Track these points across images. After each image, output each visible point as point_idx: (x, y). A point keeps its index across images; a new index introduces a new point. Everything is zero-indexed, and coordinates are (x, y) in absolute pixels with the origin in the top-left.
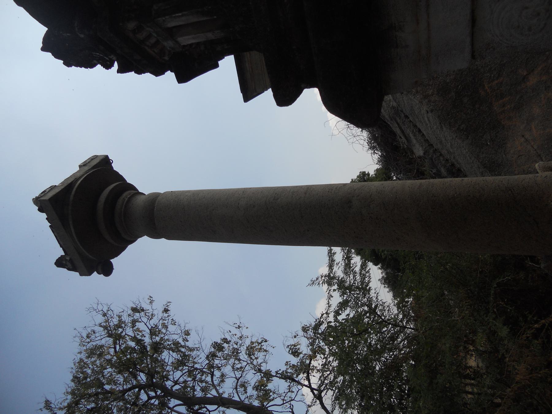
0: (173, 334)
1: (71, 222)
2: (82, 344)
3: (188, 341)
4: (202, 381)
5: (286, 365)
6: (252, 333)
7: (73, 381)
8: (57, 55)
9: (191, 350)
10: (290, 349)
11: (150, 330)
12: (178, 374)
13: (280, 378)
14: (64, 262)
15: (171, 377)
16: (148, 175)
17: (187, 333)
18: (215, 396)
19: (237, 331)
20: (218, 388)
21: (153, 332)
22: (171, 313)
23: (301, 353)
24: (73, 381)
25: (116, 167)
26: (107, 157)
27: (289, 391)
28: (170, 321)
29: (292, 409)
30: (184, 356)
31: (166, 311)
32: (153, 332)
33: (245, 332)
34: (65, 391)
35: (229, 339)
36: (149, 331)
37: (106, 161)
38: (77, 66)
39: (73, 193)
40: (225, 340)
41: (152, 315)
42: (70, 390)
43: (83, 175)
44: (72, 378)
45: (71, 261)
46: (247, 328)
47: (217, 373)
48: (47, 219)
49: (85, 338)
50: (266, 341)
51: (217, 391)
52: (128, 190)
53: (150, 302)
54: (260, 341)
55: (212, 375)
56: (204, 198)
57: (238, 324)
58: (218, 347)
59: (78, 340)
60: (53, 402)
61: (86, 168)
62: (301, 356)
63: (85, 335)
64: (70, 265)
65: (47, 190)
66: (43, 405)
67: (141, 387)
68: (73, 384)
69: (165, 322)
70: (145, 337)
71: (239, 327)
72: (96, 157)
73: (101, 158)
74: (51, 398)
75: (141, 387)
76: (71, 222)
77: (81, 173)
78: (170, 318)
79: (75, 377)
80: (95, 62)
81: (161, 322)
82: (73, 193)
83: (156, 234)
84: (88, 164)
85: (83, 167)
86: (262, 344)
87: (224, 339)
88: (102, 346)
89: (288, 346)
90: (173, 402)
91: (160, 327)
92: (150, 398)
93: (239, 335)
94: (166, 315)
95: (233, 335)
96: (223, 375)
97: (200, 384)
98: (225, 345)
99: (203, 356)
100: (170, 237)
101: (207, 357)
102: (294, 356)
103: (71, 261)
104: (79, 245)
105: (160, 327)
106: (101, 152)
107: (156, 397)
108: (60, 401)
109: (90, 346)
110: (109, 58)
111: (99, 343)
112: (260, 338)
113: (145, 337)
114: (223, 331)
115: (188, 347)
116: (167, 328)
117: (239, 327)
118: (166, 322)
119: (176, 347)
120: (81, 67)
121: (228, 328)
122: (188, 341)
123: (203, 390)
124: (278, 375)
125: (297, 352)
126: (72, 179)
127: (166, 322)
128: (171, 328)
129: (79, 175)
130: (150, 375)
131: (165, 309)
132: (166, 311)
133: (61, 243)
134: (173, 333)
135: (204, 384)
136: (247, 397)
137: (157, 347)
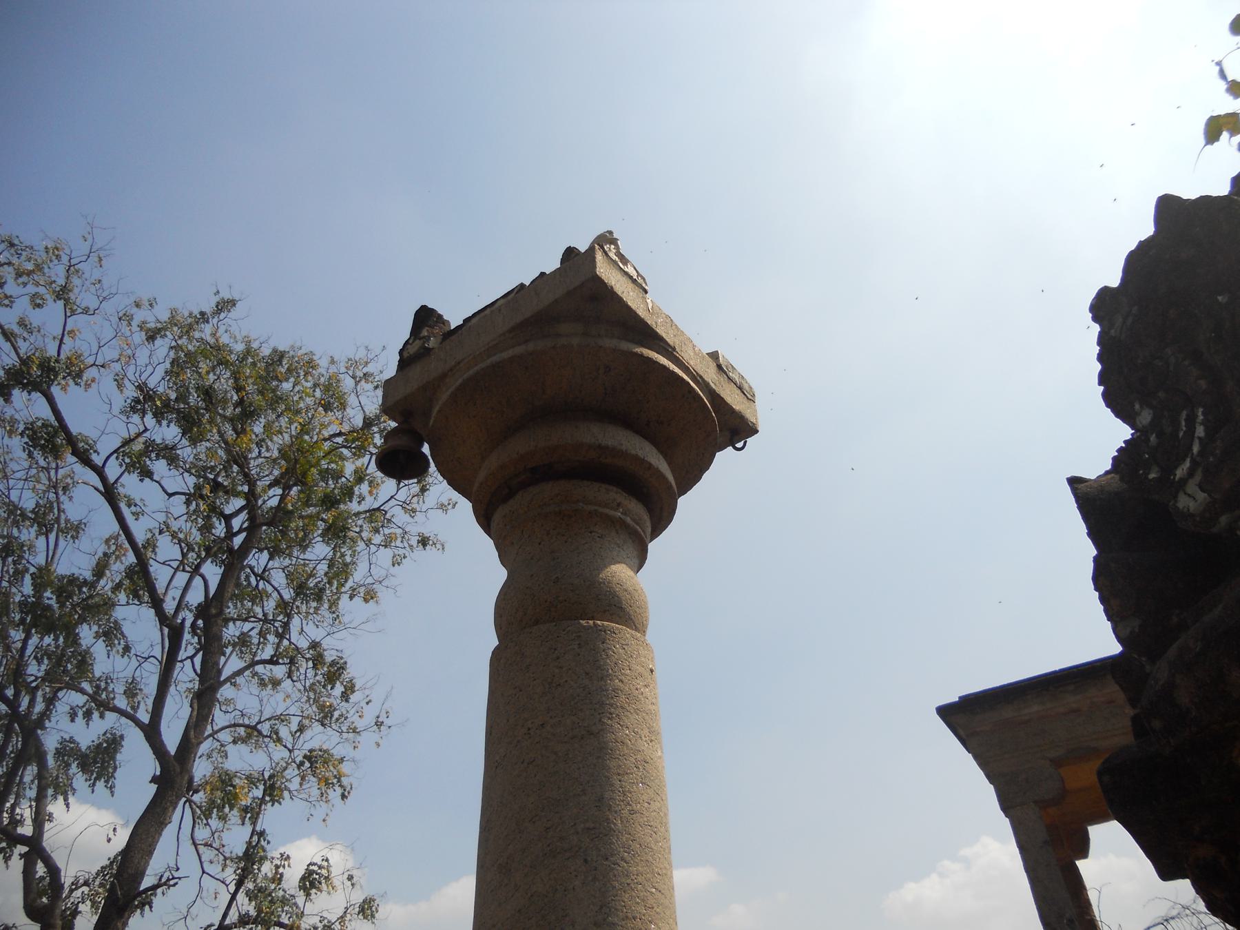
0: (369, 562)
1: (531, 346)
2: (353, 364)
3: (351, 598)
4: (262, 634)
5: (282, 855)
6: (363, 761)
7: (275, 351)
8: (1140, 261)
9: (333, 604)
10: (320, 867)
11: (378, 509)
12: (279, 578)
13: (249, 843)
14: (425, 333)
15: (276, 563)
16: (699, 578)
17: (370, 596)
18: (220, 672)
19: (369, 719)
20: (247, 673)
21: (376, 515)
22: (419, 553)
23: (308, 895)
24: (275, 351)
25: (725, 458)
26: (753, 431)
27: (225, 859)
28: (401, 552)
29: (165, 884)
30: (319, 595)
31: (424, 542)
32: (376, 515)
33: (368, 738)
34: (253, 336)
35: (353, 698)
36: (376, 506)
37: (737, 430)
38: (1101, 341)
39: (625, 346)
40: (349, 689)
41: (414, 511)
42: (255, 345)
43: (686, 369)
44: (281, 348)
45: (425, 352)
46: (378, 745)
47: (280, 671)
48: (542, 274)
49: (365, 370)
50: (343, 797)
51: (239, 673)
52: (651, 518)
53: (442, 505)
54: (345, 781)
55: (272, 661)
56: (632, 812)
57: (387, 722)
58: (335, 672)
59: (361, 354)
60: (230, 315)
61: (710, 375)
62: (300, 900)
63: (370, 368)
64: (412, 350)
65: (630, 270)
66: (226, 295)
67: (251, 497)
68: (266, 351)
69: (399, 539)
70: (359, 502)
71: (379, 724)
72: (750, 398)
73: (748, 415)
74: (235, 313)
75: (251, 497)
76: (531, 346)
77: (693, 363)
78: (407, 552)
79: (282, 355)
80: (1146, 417)
81: (399, 531)
82: (625, 346)
83: (514, 614)
84: (723, 379)
85: (713, 365)
86: (337, 788)
87: (353, 686)
88: (343, 406)
89: (327, 860)
90: (213, 572)
91: (387, 531)
92: (228, 519)
93: (360, 724)
94: (414, 541)
95: (361, 712)
96: (276, 683)
97: (256, 631)
98: (339, 689)
99: (315, 633)
100: (500, 663)
101: (314, 645)
102: (303, 879)
103: (425, 352)
104: (465, 376)
105: (387, 531)
106: (762, 413)
107: (230, 534)
108: (232, 329)
109: (348, 383)
110: (1183, 482)
111: (352, 400)
112: (351, 779)
113: (359, 502)
114: (368, 685)
115: (339, 598)
116: (386, 546)
117: (379, 724)
118: (398, 543)
119: (339, 571)
120: (1100, 358)
121: (377, 696)
122: (351, 598)
123: (243, 641)
124: (255, 838)
125: (313, 885)
126: (670, 339)
127: (398, 543)
128: (385, 555)
129: (687, 355)
130: (280, 515)
131: (428, 538)
132: (424, 542)
133: (474, 321)
134: (374, 560)
135: (255, 641)
136: (222, 745)
137: (337, 532)
